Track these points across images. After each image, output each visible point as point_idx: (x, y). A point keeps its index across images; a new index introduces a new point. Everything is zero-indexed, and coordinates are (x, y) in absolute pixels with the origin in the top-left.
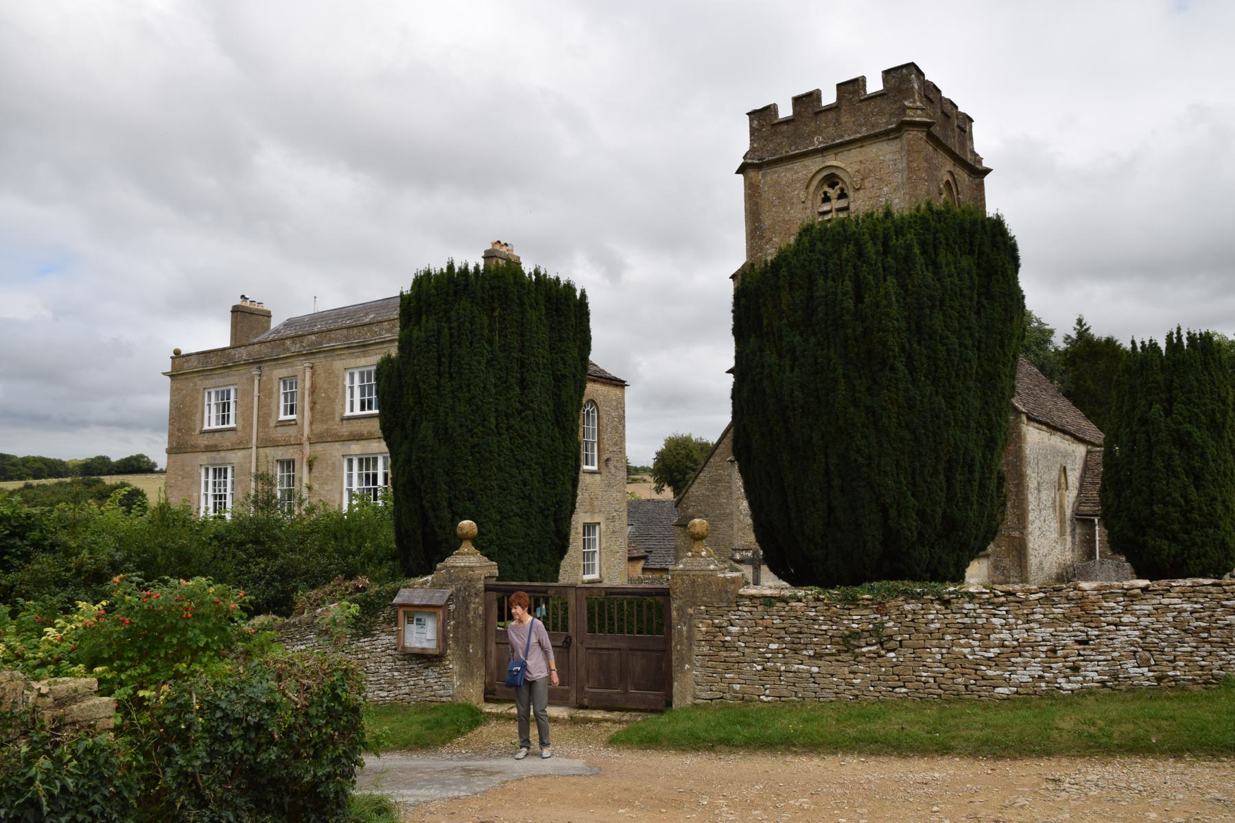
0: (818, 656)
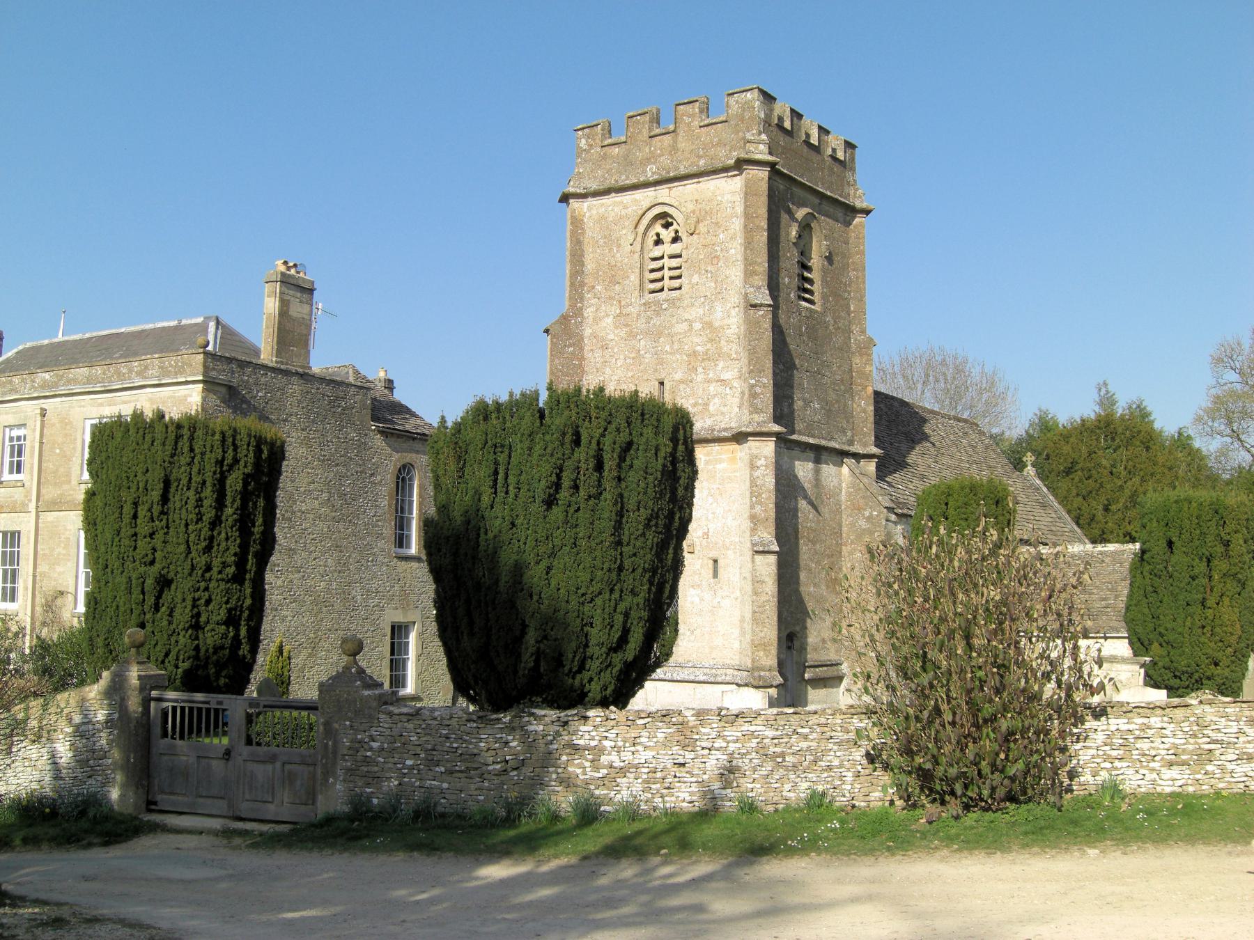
0: (450, 772)
